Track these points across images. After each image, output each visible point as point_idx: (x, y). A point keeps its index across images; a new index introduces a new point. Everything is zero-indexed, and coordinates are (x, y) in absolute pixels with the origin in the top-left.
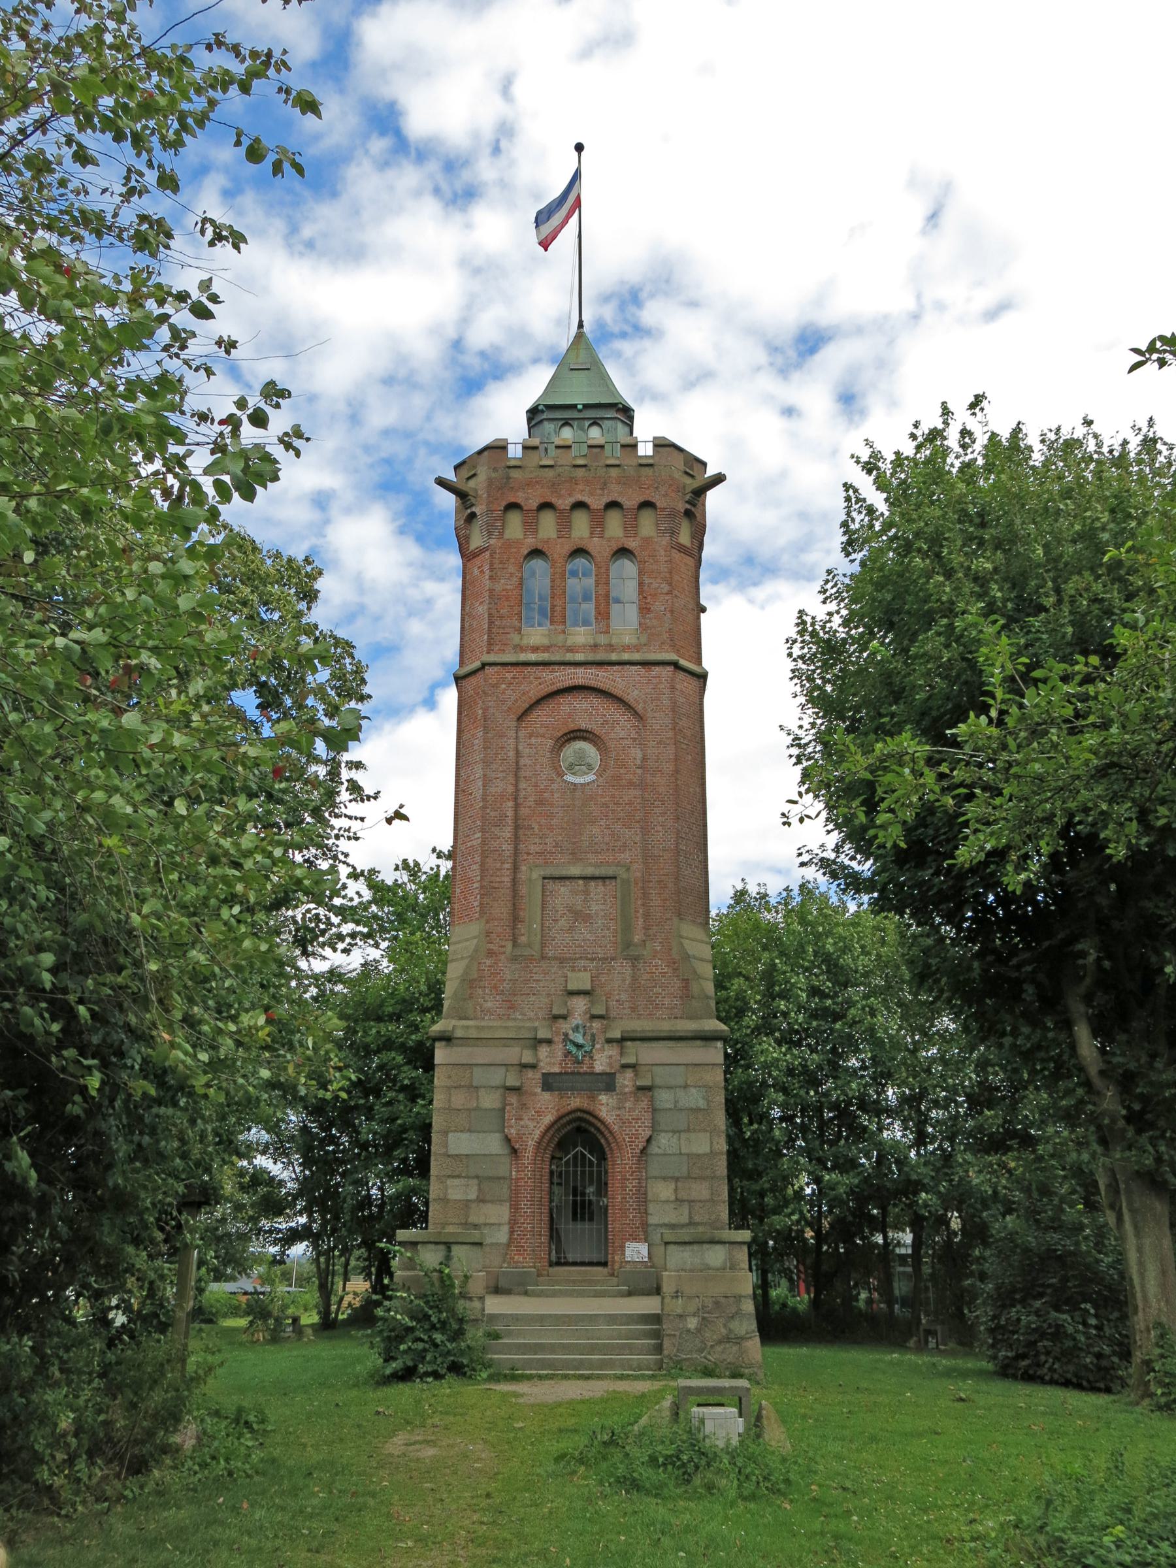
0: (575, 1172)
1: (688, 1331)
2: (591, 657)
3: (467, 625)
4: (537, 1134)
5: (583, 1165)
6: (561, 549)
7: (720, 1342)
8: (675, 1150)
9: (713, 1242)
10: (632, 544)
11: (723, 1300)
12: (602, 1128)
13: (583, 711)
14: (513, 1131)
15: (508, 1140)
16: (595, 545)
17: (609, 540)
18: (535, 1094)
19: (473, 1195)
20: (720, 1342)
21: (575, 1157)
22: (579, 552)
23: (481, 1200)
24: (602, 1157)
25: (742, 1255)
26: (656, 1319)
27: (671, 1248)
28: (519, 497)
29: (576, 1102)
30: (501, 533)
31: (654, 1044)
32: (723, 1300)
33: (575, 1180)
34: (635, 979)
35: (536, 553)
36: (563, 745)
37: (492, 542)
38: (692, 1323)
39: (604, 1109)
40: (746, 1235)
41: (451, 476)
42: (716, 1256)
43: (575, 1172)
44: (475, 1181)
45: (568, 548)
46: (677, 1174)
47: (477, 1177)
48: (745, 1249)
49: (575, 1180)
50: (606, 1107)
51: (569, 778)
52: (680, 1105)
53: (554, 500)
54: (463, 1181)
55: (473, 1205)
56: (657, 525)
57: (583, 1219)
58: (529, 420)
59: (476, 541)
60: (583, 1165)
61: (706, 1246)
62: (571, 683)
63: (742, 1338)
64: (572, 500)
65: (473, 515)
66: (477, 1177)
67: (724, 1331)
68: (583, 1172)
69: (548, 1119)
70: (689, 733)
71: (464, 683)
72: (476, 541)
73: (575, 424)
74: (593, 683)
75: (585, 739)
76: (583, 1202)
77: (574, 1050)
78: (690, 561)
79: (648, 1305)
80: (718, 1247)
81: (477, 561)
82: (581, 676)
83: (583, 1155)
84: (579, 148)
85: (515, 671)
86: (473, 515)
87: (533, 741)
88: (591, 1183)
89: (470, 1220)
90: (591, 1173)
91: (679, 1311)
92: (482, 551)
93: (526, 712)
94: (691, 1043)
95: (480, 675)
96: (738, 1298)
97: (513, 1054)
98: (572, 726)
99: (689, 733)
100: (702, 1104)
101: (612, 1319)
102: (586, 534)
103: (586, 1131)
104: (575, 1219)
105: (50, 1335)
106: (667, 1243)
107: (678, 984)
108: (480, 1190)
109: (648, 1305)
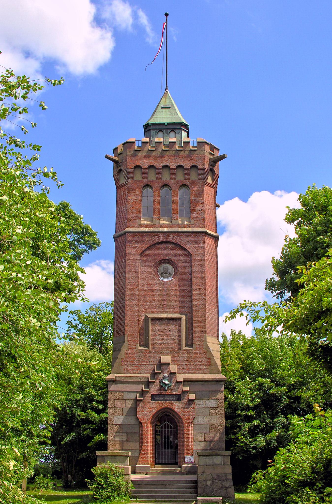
0: (165, 431)
1: (207, 485)
2: (170, 229)
3: (118, 215)
4: (150, 417)
5: (168, 428)
6: (158, 184)
7: (220, 489)
8: (204, 423)
9: (217, 455)
10: (187, 183)
11: (221, 475)
12: (175, 415)
13: (167, 252)
14: (140, 416)
15: (138, 419)
16: (172, 183)
17: (178, 181)
18: (149, 402)
19: (125, 439)
20: (220, 489)
21: (165, 425)
22: (165, 185)
23: (128, 441)
24: (176, 426)
25: (228, 460)
26: (195, 482)
27: (201, 457)
28: (141, 163)
29: (165, 405)
30: (133, 178)
31: (196, 383)
32: (221, 475)
33: (165, 433)
34: (188, 359)
35: (147, 186)
36: (159, 265)
37: (129, 181)
38: (209, 483)
39: (176, 408)
40: (230, 453)
41: (112, 155)
42: (218, 460)
43: (165, 431)
44: (126, 434)
45: (161, 184)
46: (205, 431)
47: (126, 432)
48: (229, 457)
49: (165, 433)
50: (177, 407)
51: (161, 279)
52: (206, 406)
53: (155, 165)
54: (121, 434)
55: (125, 443)
56: (198, 175)
57: (168, 448)
58: (145, 129)
59: (122, 181)
60: (168, 428)
61: (214, 457)
62: (162, 240)
63: (227, 488)
64: (163, 164)
65: (121, 170)
66: (126, 432)
67: (220, 485)
68: (168, 431)
69: (154, 411)
70: (211, 260)
71: (118, 239)
72: (122, 181)
73: (164, 131)
74: (171, 240)
75: (168, 263)
76: (168, 441)
77: (164, 386)
78: (212, 190)
79: (193, 477)
80: (219, 457)
81: (123, 189)
82: (166, 238)
83: (168, 425)
84: (166, 15)
85: (139, 235)
86: (121, 170)
87: (146, 263)
88: (171, 434)
89: (124, 448)
90: (171, 431)
91: (204, 479)
92: (125, 185)
93: (143, 252)
94: (211, 383)
95: (124, 237)
96: (226, 474)
97: (139, 387)
98: (162, 258)
99: (211, 260)
100: (215, 406)
101: (178, 482)
102: (168, 178)
103: (169, 416)
104: (165, 448)
105: (32, 439)
106: (199, 456)
107: (206, 360)
108: (127, 437)
109: (193, 477)
